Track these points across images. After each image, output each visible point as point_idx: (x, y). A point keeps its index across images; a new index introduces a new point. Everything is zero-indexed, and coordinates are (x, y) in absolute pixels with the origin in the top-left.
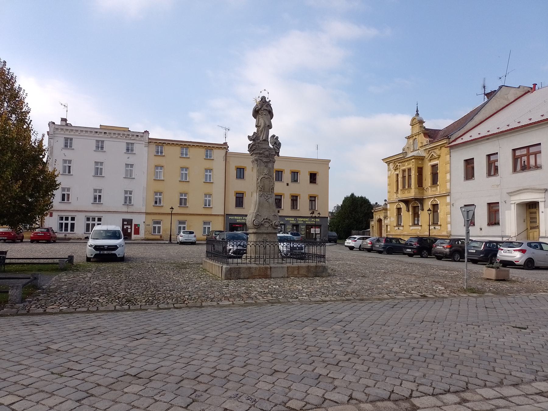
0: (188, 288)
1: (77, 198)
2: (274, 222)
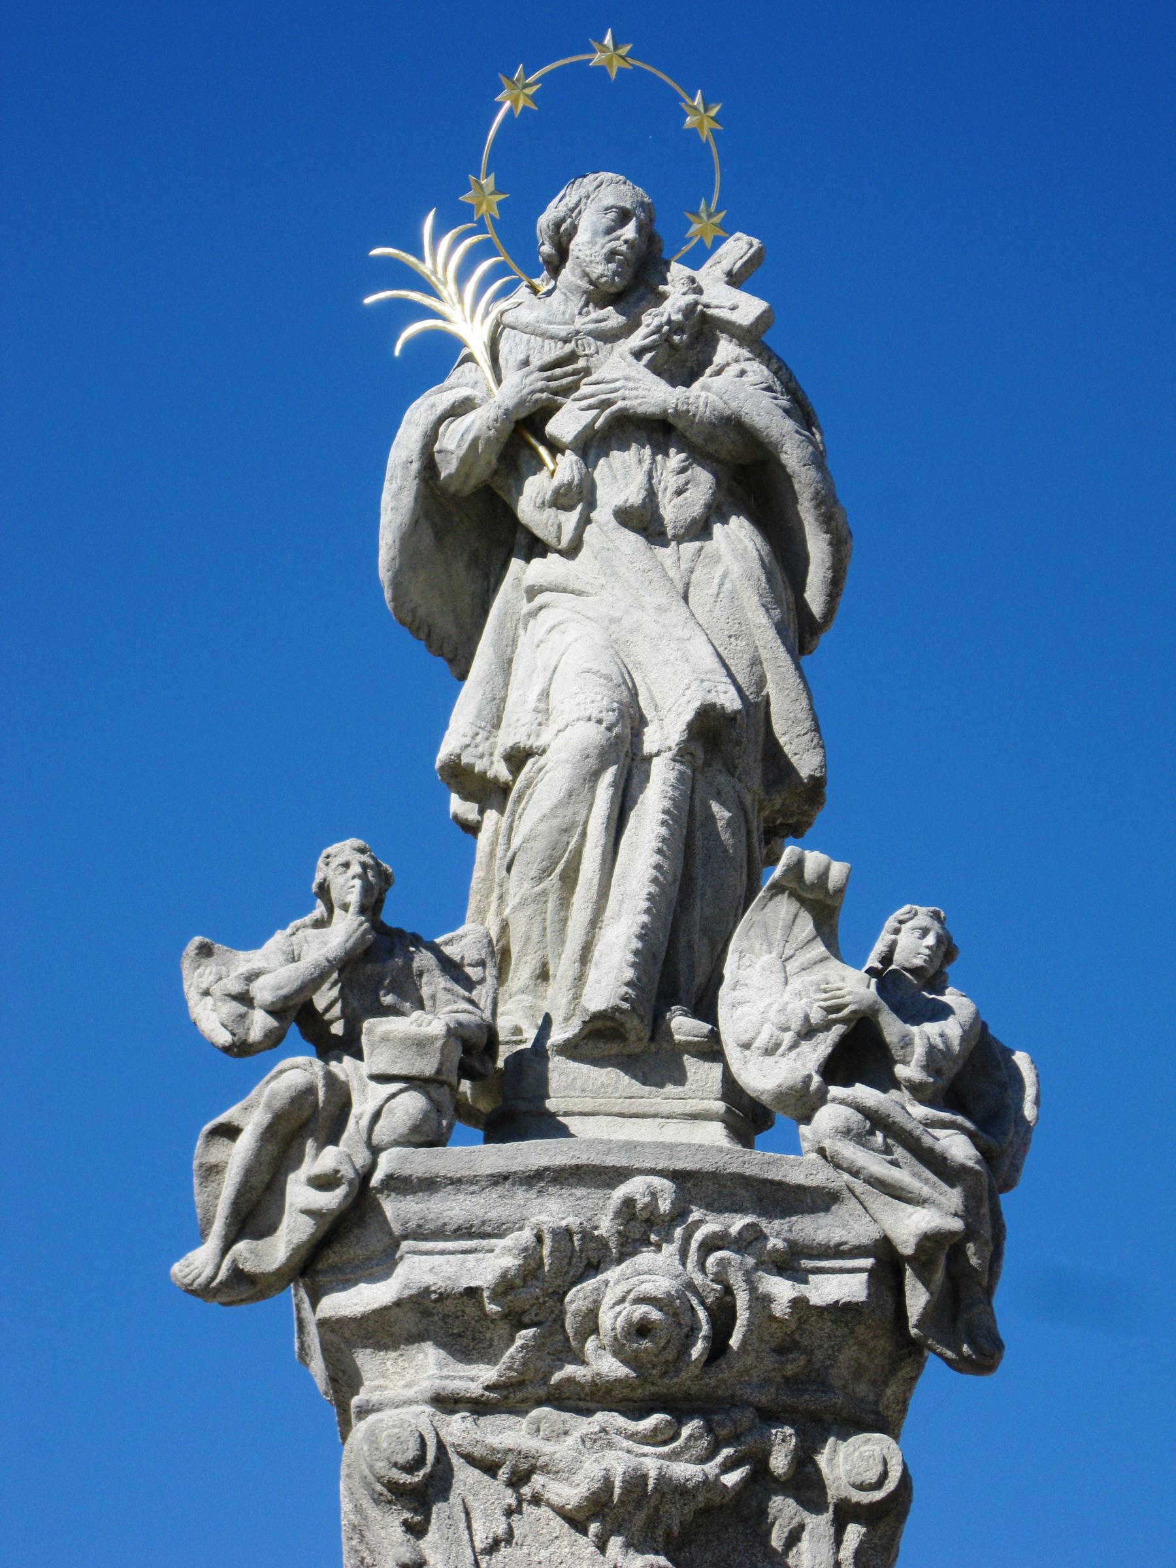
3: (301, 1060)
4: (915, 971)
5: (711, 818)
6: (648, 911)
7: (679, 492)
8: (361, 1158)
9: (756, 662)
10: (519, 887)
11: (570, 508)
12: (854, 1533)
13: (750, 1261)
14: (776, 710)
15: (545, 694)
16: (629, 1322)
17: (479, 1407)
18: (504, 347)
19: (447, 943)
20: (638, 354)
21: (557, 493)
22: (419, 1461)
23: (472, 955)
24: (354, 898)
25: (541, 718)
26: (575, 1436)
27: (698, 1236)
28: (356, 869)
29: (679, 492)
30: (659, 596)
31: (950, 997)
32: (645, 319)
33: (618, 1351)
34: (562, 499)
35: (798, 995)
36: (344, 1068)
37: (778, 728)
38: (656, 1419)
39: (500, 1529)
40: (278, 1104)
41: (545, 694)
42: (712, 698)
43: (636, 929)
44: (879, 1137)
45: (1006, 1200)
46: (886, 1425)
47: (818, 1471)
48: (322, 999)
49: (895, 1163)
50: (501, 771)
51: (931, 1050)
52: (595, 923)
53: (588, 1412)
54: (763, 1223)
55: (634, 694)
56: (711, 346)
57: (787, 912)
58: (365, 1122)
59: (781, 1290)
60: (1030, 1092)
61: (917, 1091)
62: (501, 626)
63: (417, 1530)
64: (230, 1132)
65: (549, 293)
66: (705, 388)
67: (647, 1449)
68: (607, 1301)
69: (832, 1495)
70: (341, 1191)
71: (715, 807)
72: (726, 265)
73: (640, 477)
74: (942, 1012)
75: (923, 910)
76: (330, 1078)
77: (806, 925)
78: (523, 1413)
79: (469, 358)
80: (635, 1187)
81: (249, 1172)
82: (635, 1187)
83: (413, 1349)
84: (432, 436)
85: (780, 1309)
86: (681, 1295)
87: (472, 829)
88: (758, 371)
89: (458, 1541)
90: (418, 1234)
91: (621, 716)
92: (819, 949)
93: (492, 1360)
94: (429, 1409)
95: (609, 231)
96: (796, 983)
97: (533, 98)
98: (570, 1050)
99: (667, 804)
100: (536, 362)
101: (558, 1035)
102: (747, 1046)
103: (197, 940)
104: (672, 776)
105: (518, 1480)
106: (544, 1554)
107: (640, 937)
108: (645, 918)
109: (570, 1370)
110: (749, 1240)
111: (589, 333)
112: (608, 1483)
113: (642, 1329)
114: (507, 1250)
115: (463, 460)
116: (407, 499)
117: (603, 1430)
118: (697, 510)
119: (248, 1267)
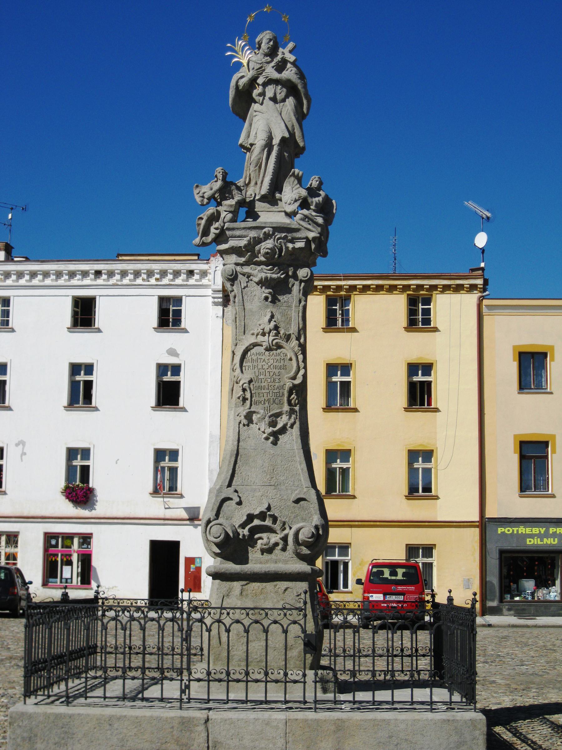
0: (155, 725)
1: (117, 463)
2: (294, 528)
3: (212, 208)
4: (315, 188)
5: (284, 155)
6: (272, 175)
7: (280, 93)
8: (222, 224)
9: (293, 126)
10: (252, 168)
11: (261, 97)
12: (303, 284)
13: (285, 241)
14: (296, 134)
15: (256, 133)
16: (265, 252)
17: (242, 265)
18: (250, 64)
19: (238, 183)
20: (273, 67)
21: (259, 94)
22: (232, 274)
23: (242, 185)
24: (221, 178)
25: (255, 138)
26: (257, 270)
27: (277, 237)
28: (221, 173)
29: (280, 93)
30: (277, 114)
31: (321, 192)
32: (275, 60)
33: (264, 256)
34: (260, 95)
35: (294, 194)
36: (219, 208)
37: (297, 138)
38: (270, 267)
39: (246, 285)
40: (208, 216)
41: (256, 133)
42: (284, 135)
43: (270, 179)
44: (307, 219)
45: (330, 228)
46: (309, 266)
47: (297, 274)
48: (216, 196)
49: (309, 224)
50: (250, 147)
51: (316, 203)
52: (264, 177)
53: (260, 266)
54: (288, 235)
55: (271, 133)
56: (286, 65)
57: (246, 268)
58: (223, 219)
59: (290, 246)
60: (335, 208)
61: (314, 211)
62: (250, 117)
63: (232, 285)
64: (201, 218)
65: (258, 54)
66: (285, 74)
67: (269, 272)
68: (262, 248)
69: (299, 278)
70: (219, 230)
71: (285, 154)
72: (289, 49)
73: (273, 91)
74: (319, 195)
75: (317, 177)
76: (217, 210)
77: (296, 182)
78: (249, 266)
79: (244, 66)
80: (266, 230)
81: (204, 227)
82: (266, 230)
83: (232, 255)
84: (237, 82)
85: (290, 249)
86: (274, 247)
87: (246, 153)
88: (294, 69)
89: (239, 287)
90: (232, 237)
91: (268, 139)
92: (298, 186)
93: (244, 257)
94: (234, 265)
95: (268, 43)
96: (294, 192)
97: (254, 18)
98: (259, 200)
99: (276, 154)
100: (255, 69)
101: (257, 198)
102: (286, 203)
103: (196, 184)
104: (277, 149)
105: (248, 277)
106: (253, 289)
107: (271, 180)
108: (272, 177)
109: (256, 259)
110: (285, 237)
111: (265, 62)
112: (262, 278)
113: (267, 253)
114: (246, 240)
115: (243, 87)
116: (234, 93)
117: (262, 269)
118: (283, 97)
119: (205, 242)
